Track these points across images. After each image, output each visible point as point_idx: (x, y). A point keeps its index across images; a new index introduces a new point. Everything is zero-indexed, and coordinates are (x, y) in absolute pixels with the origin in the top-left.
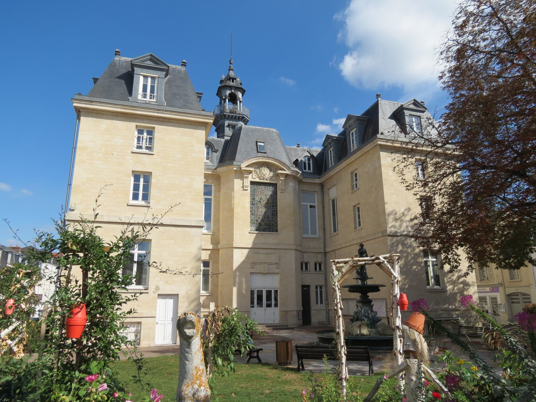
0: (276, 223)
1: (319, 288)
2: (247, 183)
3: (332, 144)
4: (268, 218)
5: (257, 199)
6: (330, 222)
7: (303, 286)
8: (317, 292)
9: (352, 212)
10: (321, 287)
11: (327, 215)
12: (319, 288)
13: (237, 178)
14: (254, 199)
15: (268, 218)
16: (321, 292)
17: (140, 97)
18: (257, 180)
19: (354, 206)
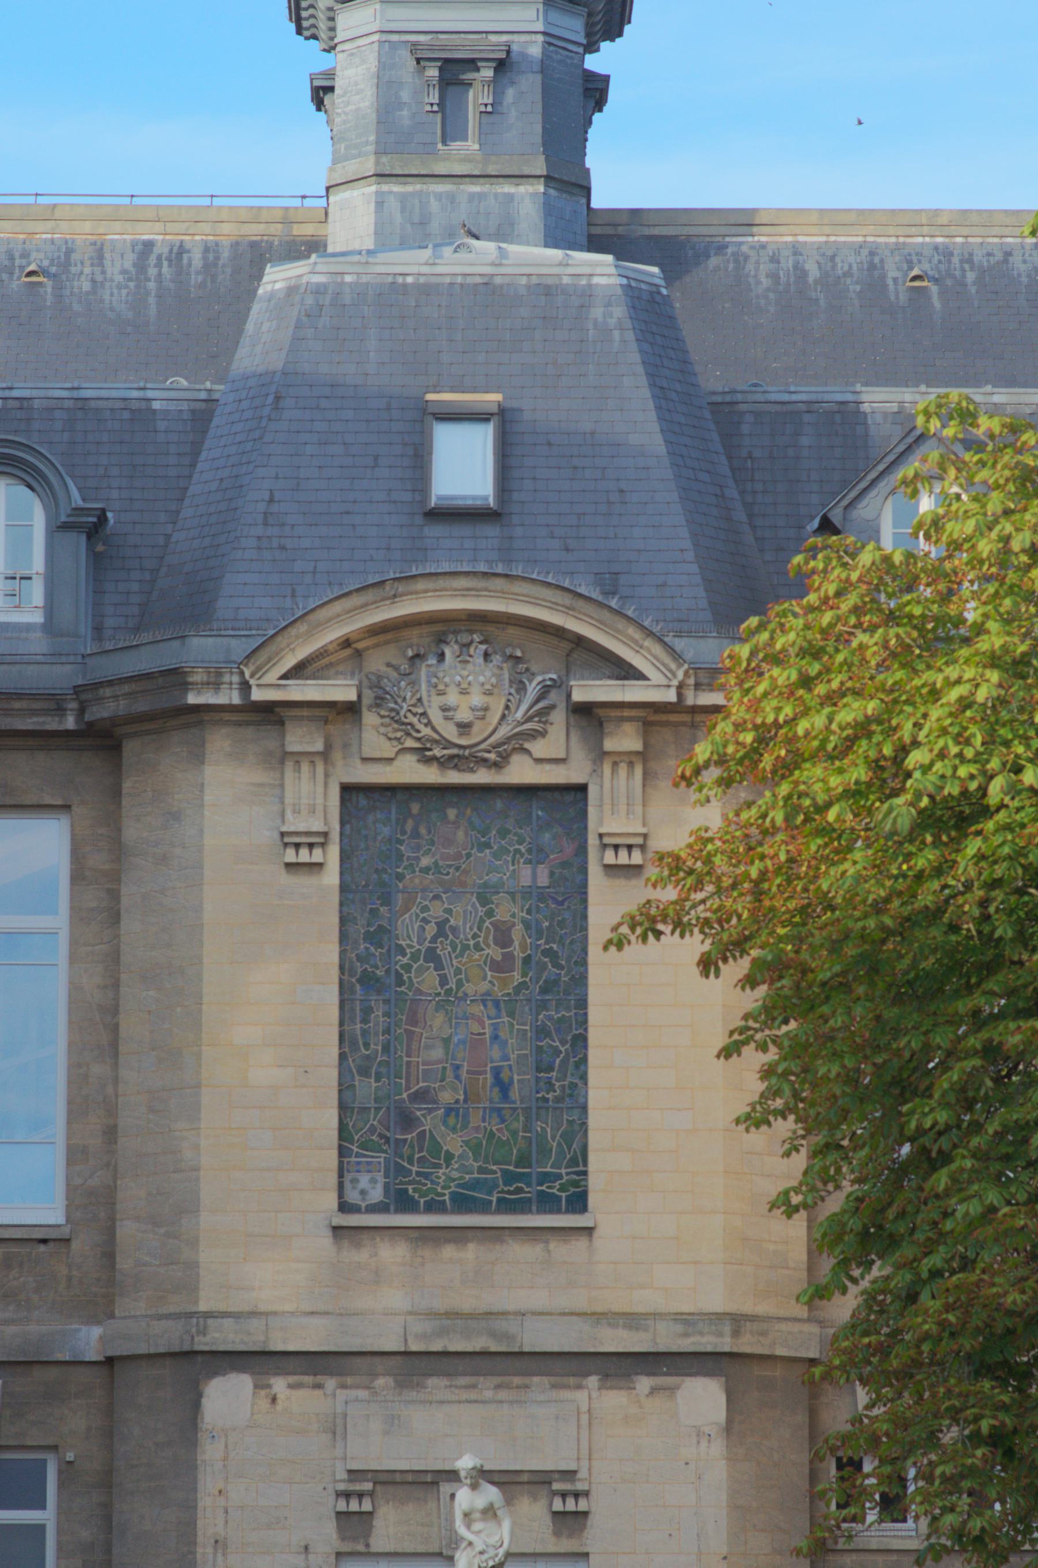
2: (312, 801)
5: (410, 930)
14: (378, 936)
15: (503, 1087)
18: (410, 771)
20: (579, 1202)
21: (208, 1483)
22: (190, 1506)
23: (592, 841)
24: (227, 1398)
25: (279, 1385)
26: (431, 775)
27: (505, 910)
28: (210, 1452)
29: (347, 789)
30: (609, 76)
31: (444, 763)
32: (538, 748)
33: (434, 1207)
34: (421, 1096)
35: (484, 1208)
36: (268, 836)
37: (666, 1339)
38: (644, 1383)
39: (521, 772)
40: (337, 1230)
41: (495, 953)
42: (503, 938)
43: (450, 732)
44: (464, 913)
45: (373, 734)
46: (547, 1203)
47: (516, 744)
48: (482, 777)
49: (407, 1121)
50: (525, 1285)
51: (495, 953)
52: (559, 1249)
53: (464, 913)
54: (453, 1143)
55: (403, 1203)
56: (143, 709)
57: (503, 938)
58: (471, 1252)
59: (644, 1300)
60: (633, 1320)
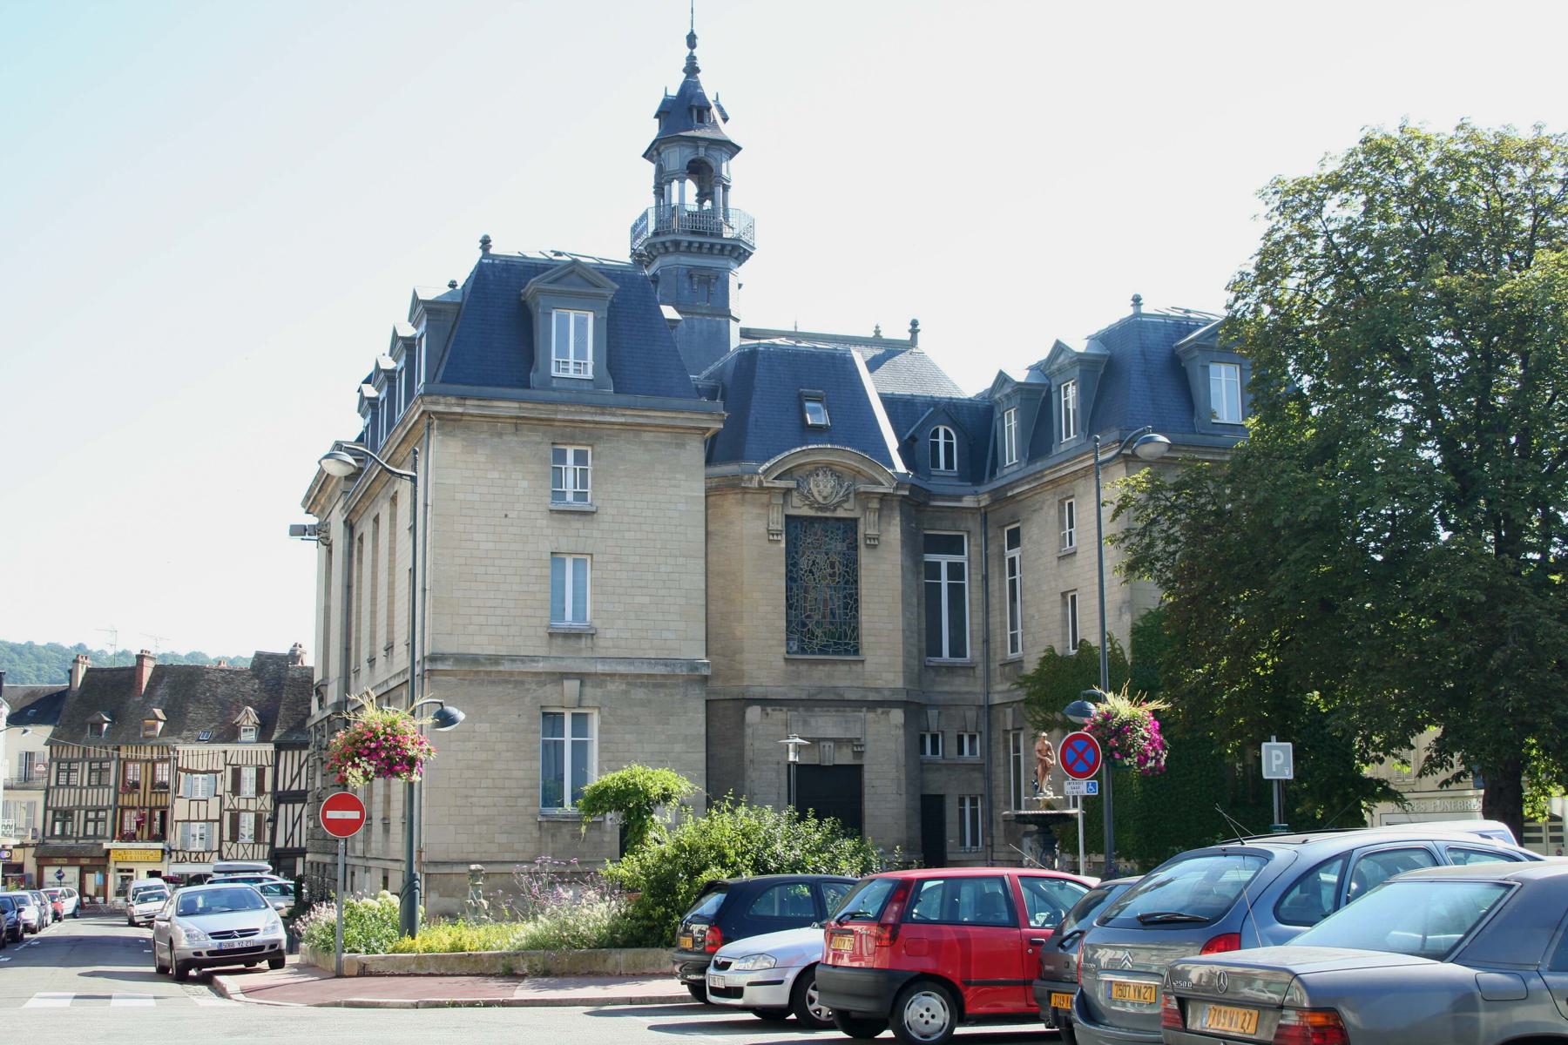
0: (855, 629)
1: (967, 803)
3: (1017, 400)
4: (833, 614)
5: (804, 563)
6: (1003, 597)
7: (924, 798)
8: (962, 812)
9: (1058, 610)
10: (974, 801)
11: (994, 601)
12: (967, 803)
13: (1132, 317)
14: (795, 565)
15: (833, 614)
16: (974, 813)
17: (590, 316)
18: (806, 511)
19: (1064, 595)
20: (856, 652)
21: (748, 741)
22: (742, 749)
23: (860, 536)
24: (753, 714)
25: (769, 710)
26: (812, 513)
27: (835, 558)
28: (749, 731)
29: (787, 517)
30: (1001, 373)
31: (818, 509)
32: (846, 505)
33: (813, 653)
34: (808, 617)
35: (827, 653)
36: (763, 530)
37: (887, 696)
38: (880, 711)
39: (840, 513)
40: (786, 660)
41: (829, 570)
42: (832, 566)
43: (820, 499)
44: (821, 559)
45: (795, 499)
46: (847, 652)
47: (839, 505)
48: (828, 514)
49: (804, 625)
50: (837, 677)
51: (829, 570)
52: (854, 667)
53: (821, 559)
54: (818, 632)
55: (803, 651)
56: (899, 536)
57: (832, 566)
58: (827, 668)
59: (880, 684)
60: (877, 690)
